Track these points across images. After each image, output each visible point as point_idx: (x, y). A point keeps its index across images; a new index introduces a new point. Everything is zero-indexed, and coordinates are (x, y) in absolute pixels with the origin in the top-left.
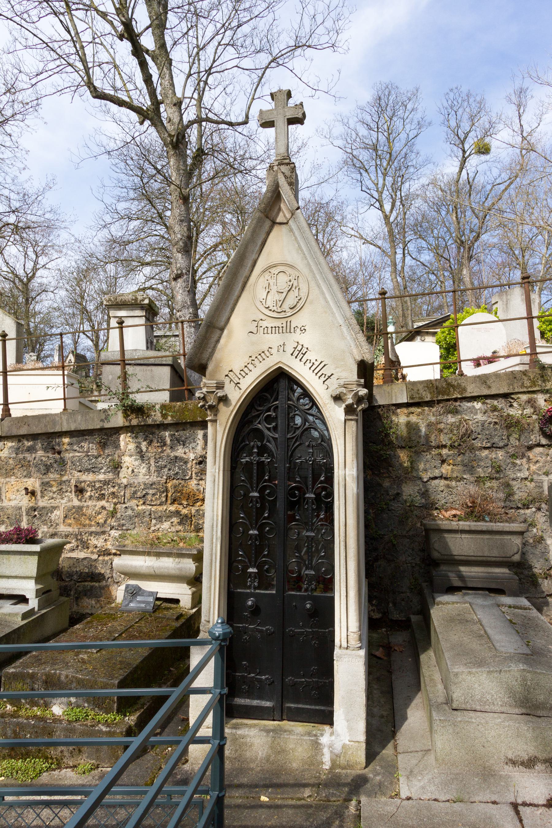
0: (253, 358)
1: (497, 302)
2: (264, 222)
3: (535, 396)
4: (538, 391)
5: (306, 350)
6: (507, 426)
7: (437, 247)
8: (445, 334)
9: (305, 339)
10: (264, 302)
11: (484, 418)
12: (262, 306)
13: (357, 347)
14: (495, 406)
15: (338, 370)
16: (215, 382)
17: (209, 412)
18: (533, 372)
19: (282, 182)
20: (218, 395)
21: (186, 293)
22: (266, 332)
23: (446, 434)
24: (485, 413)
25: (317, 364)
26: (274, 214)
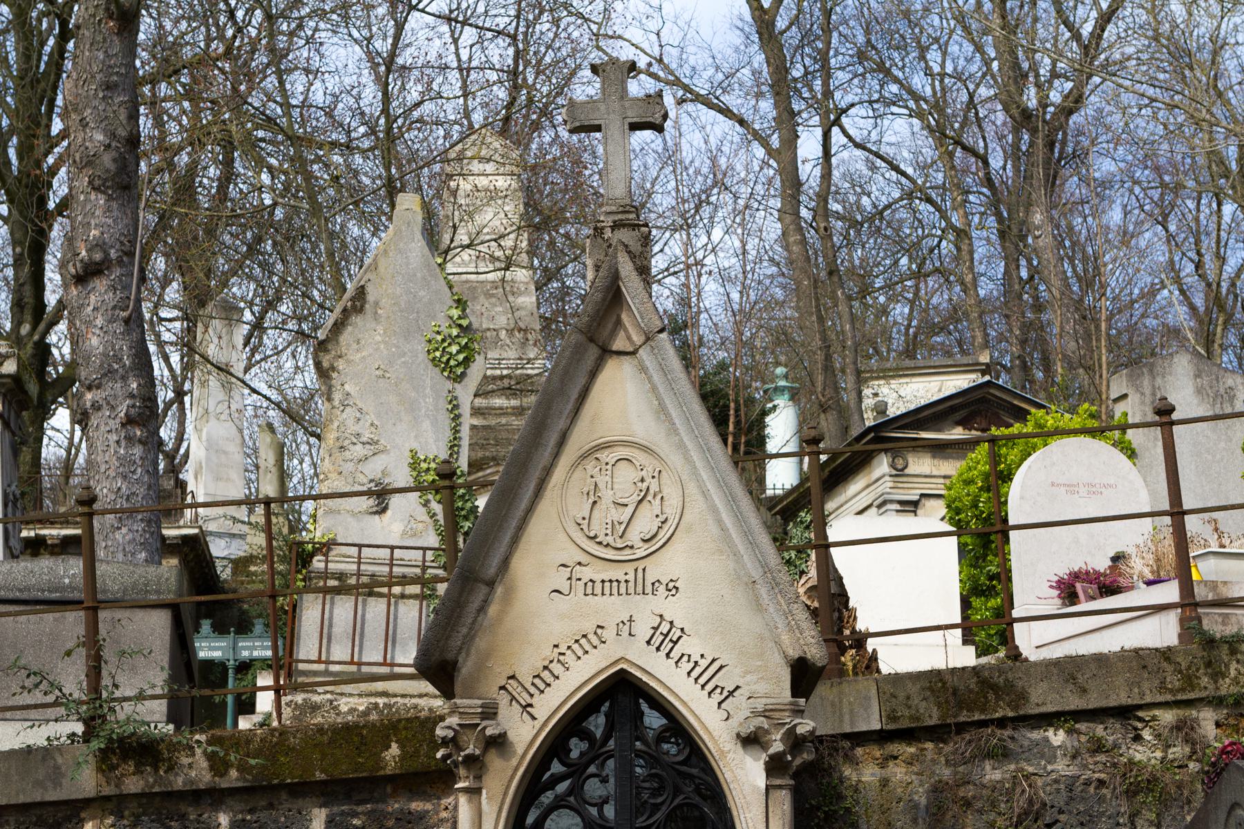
0: (563, 649)
1: (1125, 396)
2: (586, 350)
3: (1194, 713)
4: (1201, 700)
5: (679, 633)
6: (1127, 792)
7: (939, 105)
8: (973, 489)
9: (676, 610)
10: (585, 524)
11: (1072, 771)
12: (580, 534)
13: (791, 630)
14: (1099, 740)
15: (749, 678)
16: (480, 702)
17: (462, 772)
18: (1186, 653)
19: (626, 268)
20: (489, 732)
21: (119, 328)
22: (589, 591)
23: (980, 812)
24: (1074, 757)
25: (703, 663)
26: (606, 333)
